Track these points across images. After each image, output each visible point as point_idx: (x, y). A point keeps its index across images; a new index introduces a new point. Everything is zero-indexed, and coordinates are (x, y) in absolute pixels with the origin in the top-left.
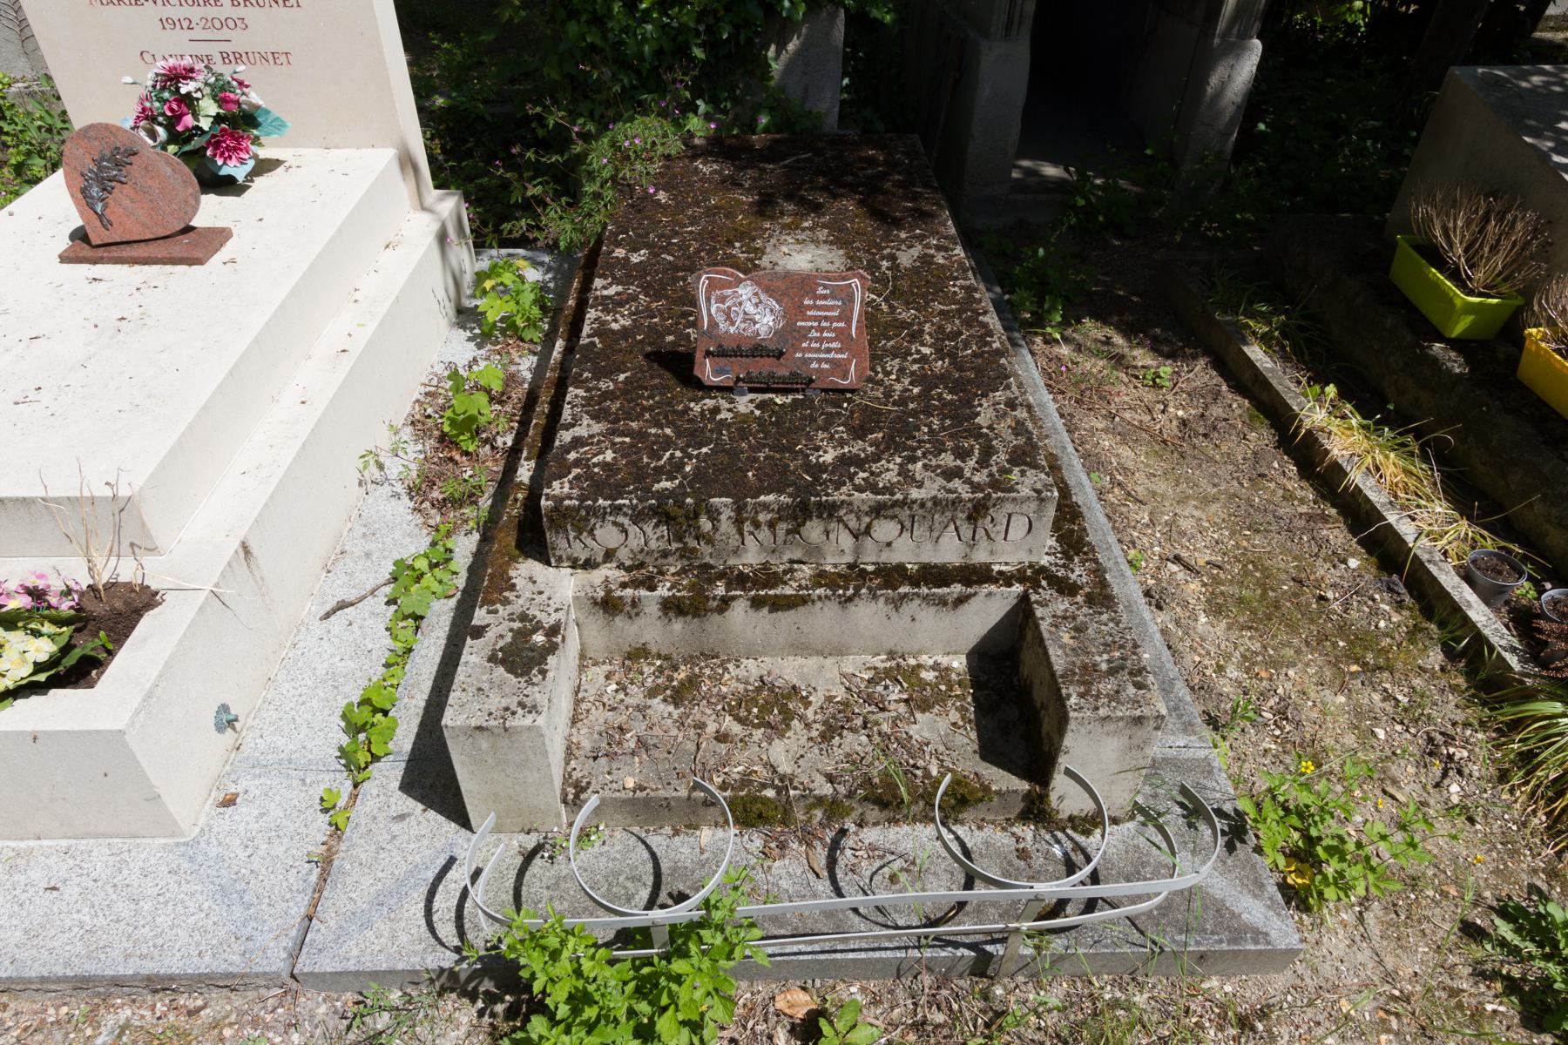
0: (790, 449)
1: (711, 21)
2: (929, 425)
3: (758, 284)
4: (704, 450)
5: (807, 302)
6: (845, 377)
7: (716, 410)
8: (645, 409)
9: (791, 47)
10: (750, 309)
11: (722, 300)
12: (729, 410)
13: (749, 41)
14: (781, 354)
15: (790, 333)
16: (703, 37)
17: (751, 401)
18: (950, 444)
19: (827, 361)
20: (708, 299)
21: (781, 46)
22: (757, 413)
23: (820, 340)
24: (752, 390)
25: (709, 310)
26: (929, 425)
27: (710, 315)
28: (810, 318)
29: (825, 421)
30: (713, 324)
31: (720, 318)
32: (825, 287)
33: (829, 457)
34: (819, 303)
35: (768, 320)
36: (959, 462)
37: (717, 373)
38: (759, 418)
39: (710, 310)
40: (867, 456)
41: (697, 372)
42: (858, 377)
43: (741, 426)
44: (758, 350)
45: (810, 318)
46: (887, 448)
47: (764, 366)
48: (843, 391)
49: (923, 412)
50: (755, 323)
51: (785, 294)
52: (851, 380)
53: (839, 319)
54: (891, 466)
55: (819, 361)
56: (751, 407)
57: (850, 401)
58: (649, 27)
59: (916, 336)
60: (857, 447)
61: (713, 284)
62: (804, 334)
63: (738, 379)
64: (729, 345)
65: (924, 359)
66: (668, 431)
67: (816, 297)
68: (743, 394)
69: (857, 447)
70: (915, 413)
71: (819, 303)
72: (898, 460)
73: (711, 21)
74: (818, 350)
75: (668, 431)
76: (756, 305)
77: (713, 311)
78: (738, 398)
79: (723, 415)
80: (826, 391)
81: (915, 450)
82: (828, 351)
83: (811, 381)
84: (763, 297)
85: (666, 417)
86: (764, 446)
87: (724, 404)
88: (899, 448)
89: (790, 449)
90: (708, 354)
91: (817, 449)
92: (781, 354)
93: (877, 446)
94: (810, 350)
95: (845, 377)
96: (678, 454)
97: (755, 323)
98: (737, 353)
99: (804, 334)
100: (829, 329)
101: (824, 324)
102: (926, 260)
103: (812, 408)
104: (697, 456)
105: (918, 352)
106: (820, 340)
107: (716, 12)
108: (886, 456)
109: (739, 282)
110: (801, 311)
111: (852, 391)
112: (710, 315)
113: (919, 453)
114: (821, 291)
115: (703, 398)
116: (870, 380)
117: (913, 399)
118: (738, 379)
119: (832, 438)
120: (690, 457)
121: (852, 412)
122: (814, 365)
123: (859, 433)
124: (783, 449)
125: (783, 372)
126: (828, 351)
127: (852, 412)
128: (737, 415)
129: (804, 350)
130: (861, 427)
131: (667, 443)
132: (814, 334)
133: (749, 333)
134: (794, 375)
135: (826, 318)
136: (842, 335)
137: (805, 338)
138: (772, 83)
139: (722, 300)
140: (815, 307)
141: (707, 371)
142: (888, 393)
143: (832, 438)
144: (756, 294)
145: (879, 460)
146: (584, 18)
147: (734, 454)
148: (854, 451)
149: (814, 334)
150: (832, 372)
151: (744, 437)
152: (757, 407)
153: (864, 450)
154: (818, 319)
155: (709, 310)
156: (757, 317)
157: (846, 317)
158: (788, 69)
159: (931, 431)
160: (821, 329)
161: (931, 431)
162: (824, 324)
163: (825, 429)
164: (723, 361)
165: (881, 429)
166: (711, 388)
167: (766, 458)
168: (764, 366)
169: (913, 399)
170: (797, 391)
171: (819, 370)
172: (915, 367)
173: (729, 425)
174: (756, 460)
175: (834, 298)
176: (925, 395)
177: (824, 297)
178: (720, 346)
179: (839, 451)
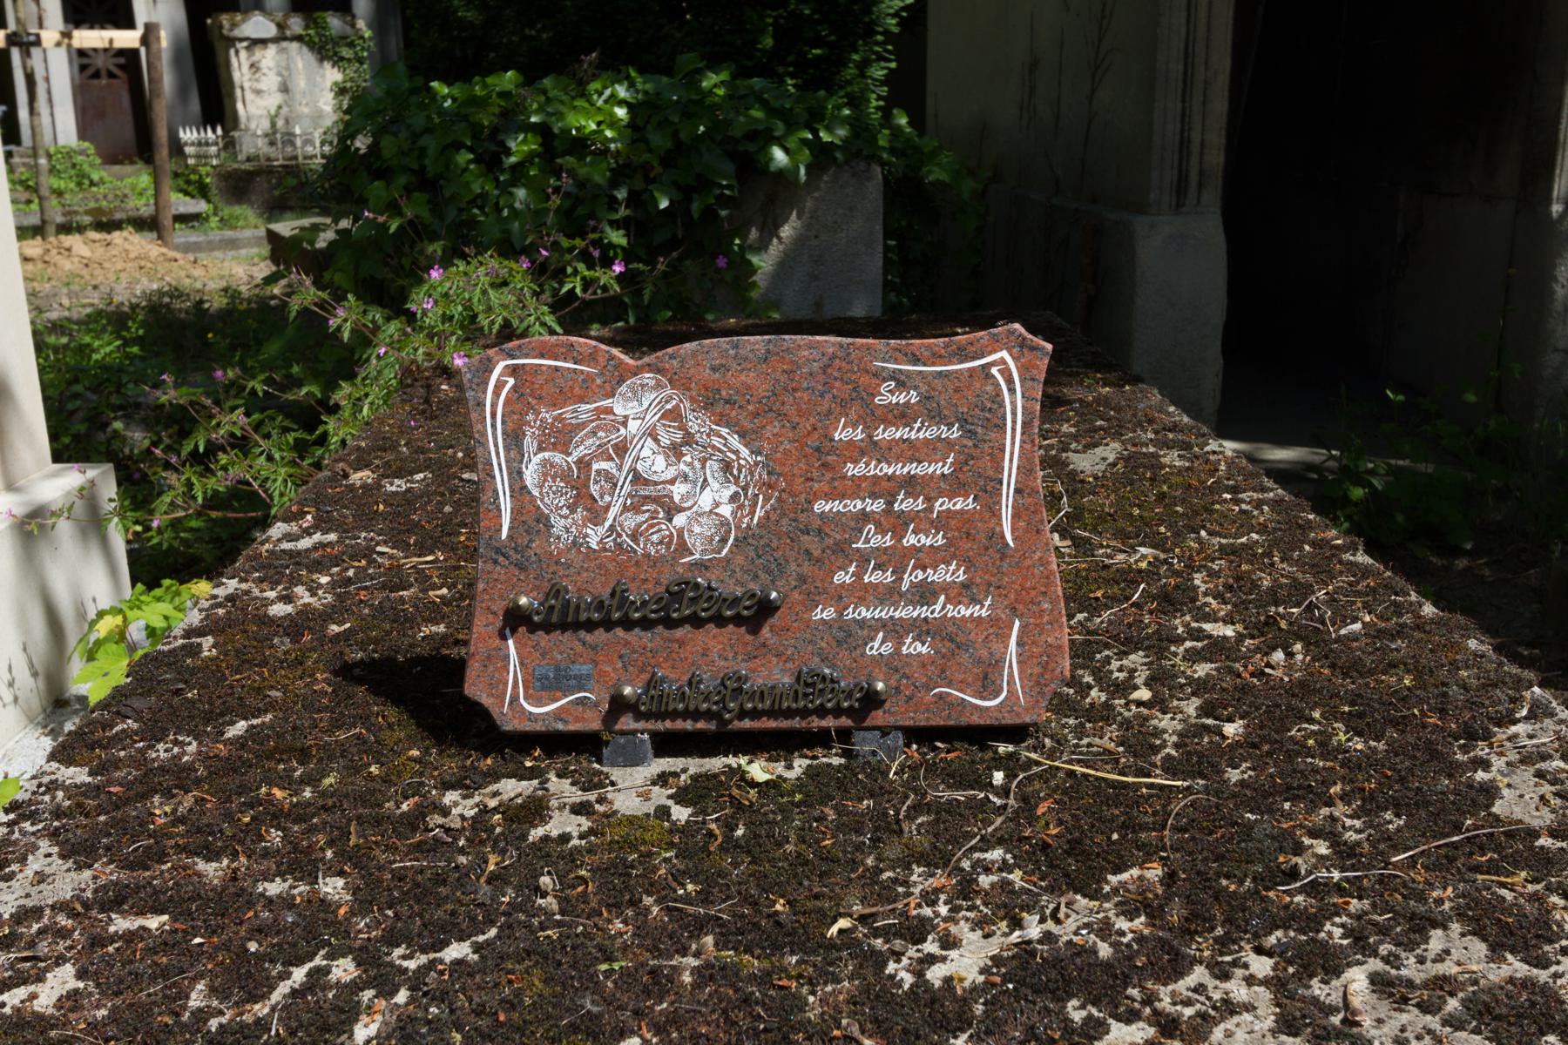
0: (802, 934)
1: (639, 184)
2: (1329, 832)
3: (678, 381)
4: (456, 951)
5: (843, 433)
6: (987, 686)
7: (535, 810)
8: (277, 816)
9: (786, 231)
10: (655, 464)
11: (560, 437)
12: (580, 809)
13: (709, 213)
14: (765, 609)
15: (789, 540)
16: (623, 212)
17: (662, 779)
18: (1445, 896)
19: (923, 629)
20: (514, 439)
21: (770, 230)
22: (681, 814)
23: (895, 559)
24: (666, 745)
25: (516, 475)
26: (1329, 832)
27: (519, 490)
28: (858, 487)
29: (932, 829)
30: (531, 520)
31: (552, 500)
32: (902, 383)
33: (967, 960)
34: (883, 434)
35: (716, 497)
36: (1516, 967)
37: (545, 684)
38: (686, 830)
39: (519, 474)
40: (1125, 955)
41: (475, 689)
42: (1036, 683)
43: (620, 860)
44: (684, 605)
45: (858, 487)
46: (1196, 923)
47: (711, 655)
48: (981, 735)
49: (1289, 793)
50: (672, 510)
51: (768, 409)
52: (1010, 693)
53: (955, 485)
54: (1238, 990)
55: (896, 630)
56: (660, 795)
57: (1010, 765)
58: (521, 193)
59: (1175, 599)
60: (1074, 921)
61: (527, 391)
62: (838, 543)
63: (619, 706)
64: (586, 588)
65: (1217, 649)
66: (332, 887)
67: (875, 417)
68: (635, 761)
69: (1074, 921)
70: (1258, 796)
71: (883, 434)
72: (1262, 966)
73: (639, 184)
74: (890, 594)
75: (332, 887)
76: (675, 451)
77: (530, 475)
78: (616, 774)
79: (561, 824)
80: (920, 735)
81: (1311, 922)
82: (925, 594)
83: (872, 700)
84: (697, 423)
85: (338, 839)
86: (700, 926)
87: (562, 789)
88: (1242, 923)
89: (802, 934)
90: (515, 620)
91: (916, 931)
92: (765, 609)
93: (1154, 913)
94: (863, 594)
95: (987, 686)
96: (344, 970)
97: (672, 510)
98: (614, 614)
99: (838, 543)
100: (922, 521)
101: (904, 504)
102: (1135, 466)
103: (879, 792)
104: (416, 982)
105: (1197, 635)
106: (895, 559)
107: (646, 168)
108: (1201, 946)
109: (615, 379)
110: (825, 460)
111: (1016, 733)
112: (519, 490)
113: (1334, 932)
114: (887, 396)
115: (495, 776)
116: (1061, 706)
117: (1233, 755)
118: (619, 706)
119: (966, 889)
120: (383, 979)
121: (1028, 803)
122: (879, 647)
123: (1073, 866)
124: (777, 938)
125: (775, 675)
126: (925, 594)
127: (1028, 803)
128: (603, 821)
129: (840, 597)
130: (1075, 847)
131: (315, 928)
132: (876, 540)
133: (651, 546)
134: (809, 682)
135: (911, 484)
136: (970, 539)
137: (842, 552)
138: (754, 294)
139: (560, 437)
140: (870, 449)
141: (514, 684)
142: (1140, 742)
143: (966, 889)
144: (673, 415)
145: (1177, 967)
146: (402, 180)
147: (570, 962)
148: (1066, 931)
149: (876, 540)
150: (940, 668)
151: (621, 898)
152: (681, 798)
153: (1105, 930)
154: (886, 489)
155: (516, 475)
156: (678, 490)
157: (976, 475)
158: (784, 267)
159: (1344, 853)
160: (897, 523)
161: (1344, 853)
162: (904, 504)
163: (934, 859)
164: (565, 642)
165: (1148, 853)
166: (524, 742)
167: (705, 974)
168: (711, 655)
169: (1233, 755)
170: (822, 739)
171: (893, 664)
172: (1202, 670)
173: (573, 857)
174: (661, 983)
175: (936, 417)
176: (1267, 740)
177: (902, 416)
178: (556, 591)
179: (1003, 940)
